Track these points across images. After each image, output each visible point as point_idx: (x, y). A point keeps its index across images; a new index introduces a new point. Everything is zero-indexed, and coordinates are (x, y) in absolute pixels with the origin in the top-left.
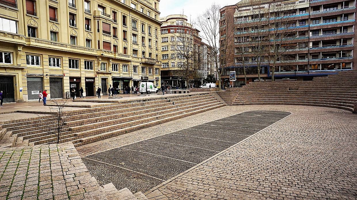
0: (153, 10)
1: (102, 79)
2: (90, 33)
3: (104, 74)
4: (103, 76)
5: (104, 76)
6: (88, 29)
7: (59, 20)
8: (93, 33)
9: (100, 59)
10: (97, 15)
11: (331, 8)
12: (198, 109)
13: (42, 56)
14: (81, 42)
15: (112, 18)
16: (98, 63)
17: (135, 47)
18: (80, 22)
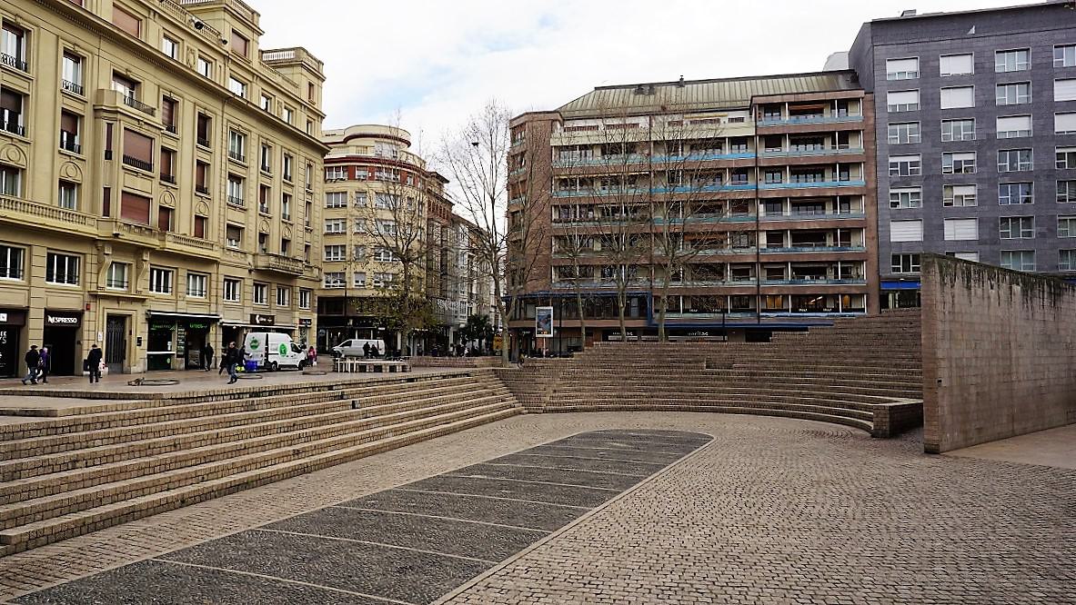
6: (70, 146)
10: (107, 104)
13: (177, 273)
16: (100, 263)
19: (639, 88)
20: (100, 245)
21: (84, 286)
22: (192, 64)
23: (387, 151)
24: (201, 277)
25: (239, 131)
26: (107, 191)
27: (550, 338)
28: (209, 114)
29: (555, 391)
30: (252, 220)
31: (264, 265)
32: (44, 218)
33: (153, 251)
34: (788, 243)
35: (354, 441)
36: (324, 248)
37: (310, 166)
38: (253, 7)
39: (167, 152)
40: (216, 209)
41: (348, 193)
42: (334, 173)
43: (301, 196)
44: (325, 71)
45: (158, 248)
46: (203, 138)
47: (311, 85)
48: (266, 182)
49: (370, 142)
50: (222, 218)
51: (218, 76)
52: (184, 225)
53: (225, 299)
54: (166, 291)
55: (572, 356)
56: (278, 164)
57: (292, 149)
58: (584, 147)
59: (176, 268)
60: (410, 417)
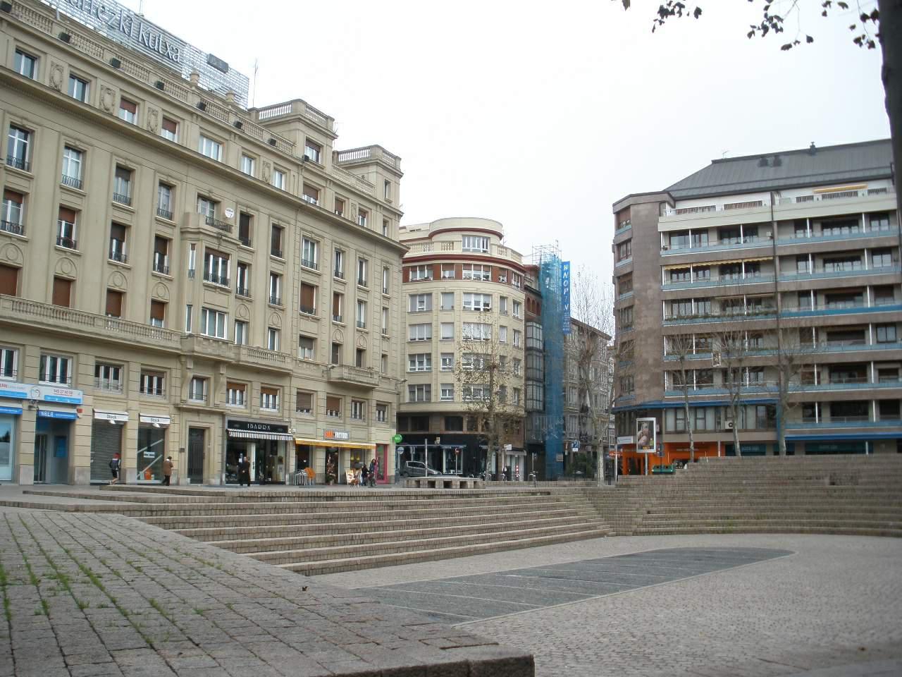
0: (377, 204)
1: (193, 430)
2: (165, 282)
3: (198, 412)
4: (196, 418)
5: (199, 422)
6: (161, 269)
7: (81, 245)
8: (175, 284)
9: (190, 365)
10: (192, 225)
11: (680, 275)
12: (500, 538)
13: (251, 386)
14: (137, 309)
15: (235, 233)
16: (183, 377)
17: (309, 328)
18: (140, 247)
19: (763, 160)
20: (183, 360)
21: (170, 400)
22: (267, 178)
23: (474, 247)
24: (313, 245)
25: (311, 238)
28: (282, 224)
29: (649, 512)
31: (338, 377)
32: (125, 333)
33: (230, 366)
35: (407, 547)
36: (407, 357)
37: (386, 269)
38: (327, 113)
39: (243, 265)
40: (289, 320)
41: (433, 295)
42: (418, 272)
43: (377, 302)
44: (403, 167)
45: (233, 362)
46: (276, 249)
47: (387, 183)
48: (339, 289)
49: (457, 237)
50: (294, 328)
51: (292, 187)
56: (352, 269)
57: (367, 251)
58: (697, 232)
59: (250, 381)
60: (470, 531)
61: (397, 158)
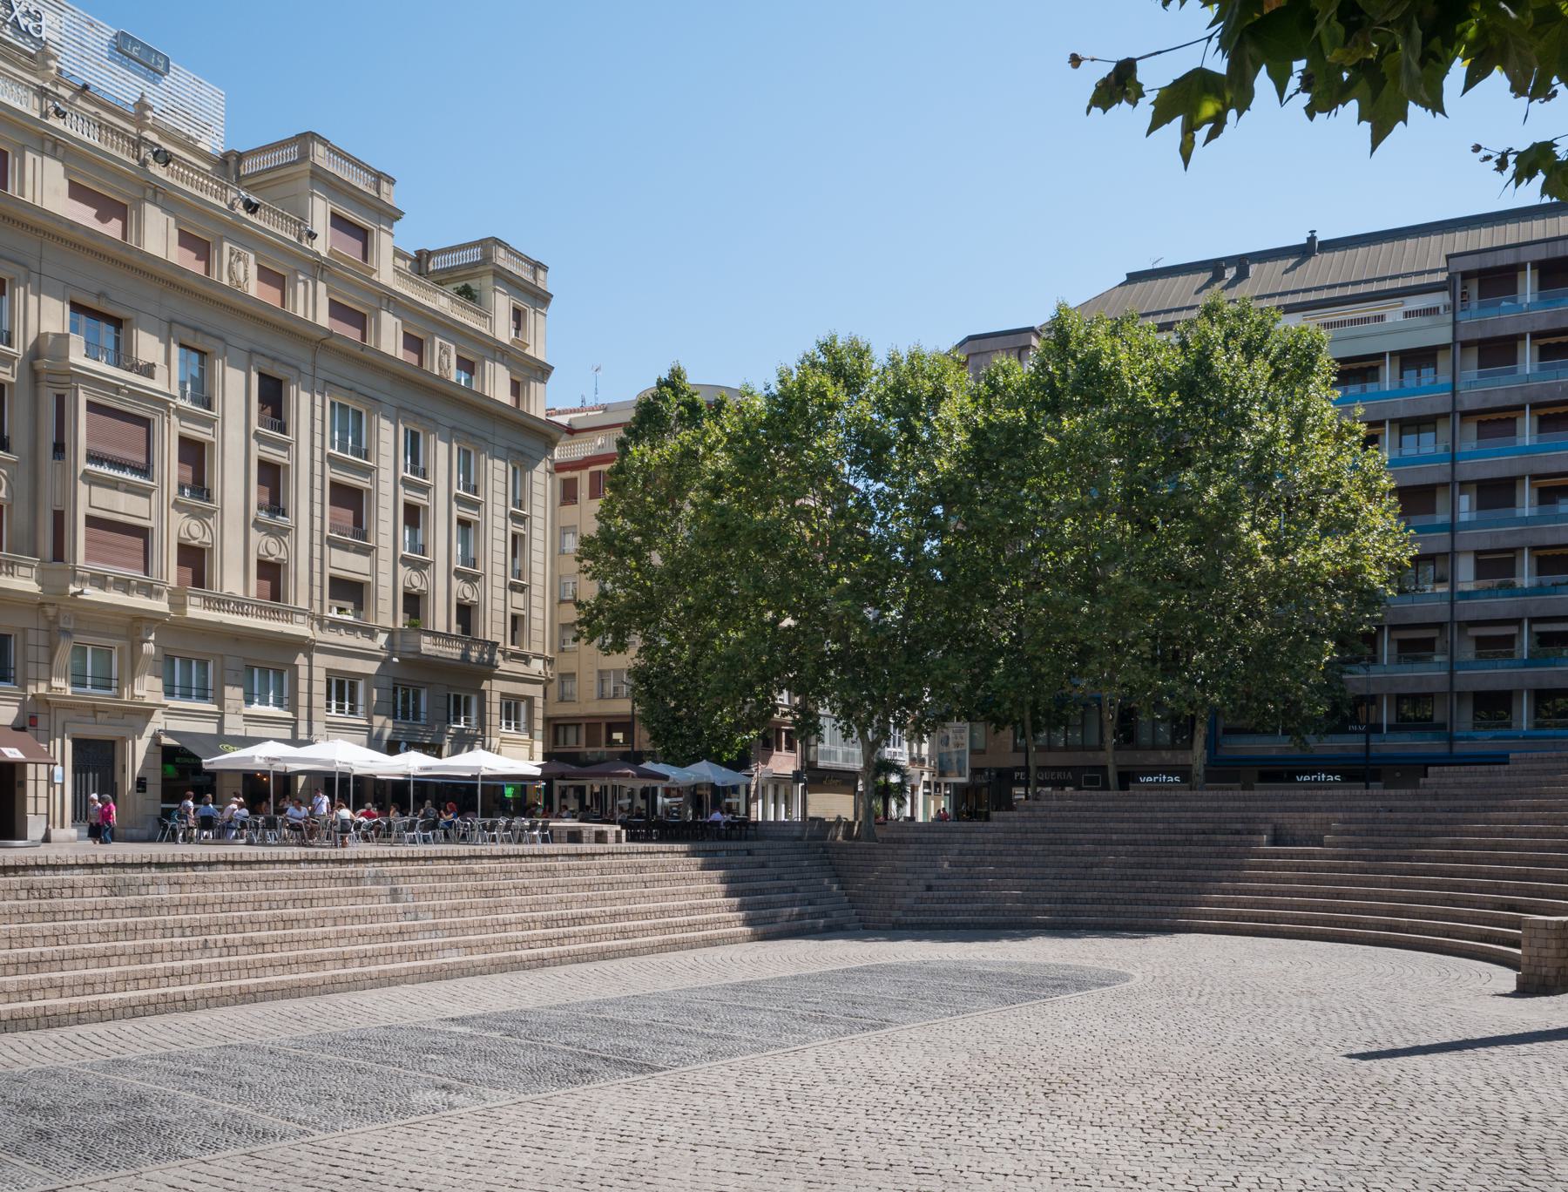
26: (59, 517)
27: (962, 784)
29: (929, 888)
30: (385, 567)
34: (1526, 578)
52: (233, 577)
53: (504, 729)
54: (353, 710)
55: (987, 819)
61: (537, 266)
